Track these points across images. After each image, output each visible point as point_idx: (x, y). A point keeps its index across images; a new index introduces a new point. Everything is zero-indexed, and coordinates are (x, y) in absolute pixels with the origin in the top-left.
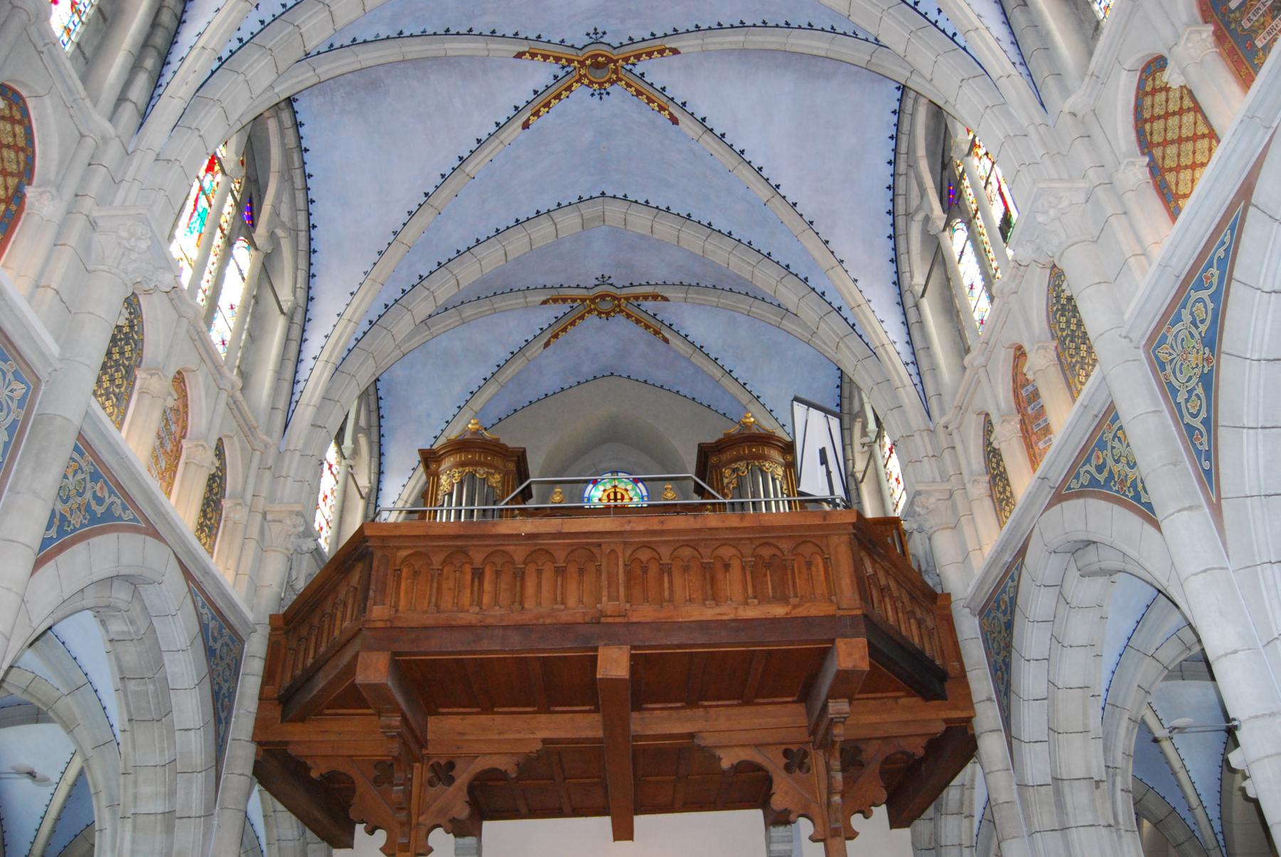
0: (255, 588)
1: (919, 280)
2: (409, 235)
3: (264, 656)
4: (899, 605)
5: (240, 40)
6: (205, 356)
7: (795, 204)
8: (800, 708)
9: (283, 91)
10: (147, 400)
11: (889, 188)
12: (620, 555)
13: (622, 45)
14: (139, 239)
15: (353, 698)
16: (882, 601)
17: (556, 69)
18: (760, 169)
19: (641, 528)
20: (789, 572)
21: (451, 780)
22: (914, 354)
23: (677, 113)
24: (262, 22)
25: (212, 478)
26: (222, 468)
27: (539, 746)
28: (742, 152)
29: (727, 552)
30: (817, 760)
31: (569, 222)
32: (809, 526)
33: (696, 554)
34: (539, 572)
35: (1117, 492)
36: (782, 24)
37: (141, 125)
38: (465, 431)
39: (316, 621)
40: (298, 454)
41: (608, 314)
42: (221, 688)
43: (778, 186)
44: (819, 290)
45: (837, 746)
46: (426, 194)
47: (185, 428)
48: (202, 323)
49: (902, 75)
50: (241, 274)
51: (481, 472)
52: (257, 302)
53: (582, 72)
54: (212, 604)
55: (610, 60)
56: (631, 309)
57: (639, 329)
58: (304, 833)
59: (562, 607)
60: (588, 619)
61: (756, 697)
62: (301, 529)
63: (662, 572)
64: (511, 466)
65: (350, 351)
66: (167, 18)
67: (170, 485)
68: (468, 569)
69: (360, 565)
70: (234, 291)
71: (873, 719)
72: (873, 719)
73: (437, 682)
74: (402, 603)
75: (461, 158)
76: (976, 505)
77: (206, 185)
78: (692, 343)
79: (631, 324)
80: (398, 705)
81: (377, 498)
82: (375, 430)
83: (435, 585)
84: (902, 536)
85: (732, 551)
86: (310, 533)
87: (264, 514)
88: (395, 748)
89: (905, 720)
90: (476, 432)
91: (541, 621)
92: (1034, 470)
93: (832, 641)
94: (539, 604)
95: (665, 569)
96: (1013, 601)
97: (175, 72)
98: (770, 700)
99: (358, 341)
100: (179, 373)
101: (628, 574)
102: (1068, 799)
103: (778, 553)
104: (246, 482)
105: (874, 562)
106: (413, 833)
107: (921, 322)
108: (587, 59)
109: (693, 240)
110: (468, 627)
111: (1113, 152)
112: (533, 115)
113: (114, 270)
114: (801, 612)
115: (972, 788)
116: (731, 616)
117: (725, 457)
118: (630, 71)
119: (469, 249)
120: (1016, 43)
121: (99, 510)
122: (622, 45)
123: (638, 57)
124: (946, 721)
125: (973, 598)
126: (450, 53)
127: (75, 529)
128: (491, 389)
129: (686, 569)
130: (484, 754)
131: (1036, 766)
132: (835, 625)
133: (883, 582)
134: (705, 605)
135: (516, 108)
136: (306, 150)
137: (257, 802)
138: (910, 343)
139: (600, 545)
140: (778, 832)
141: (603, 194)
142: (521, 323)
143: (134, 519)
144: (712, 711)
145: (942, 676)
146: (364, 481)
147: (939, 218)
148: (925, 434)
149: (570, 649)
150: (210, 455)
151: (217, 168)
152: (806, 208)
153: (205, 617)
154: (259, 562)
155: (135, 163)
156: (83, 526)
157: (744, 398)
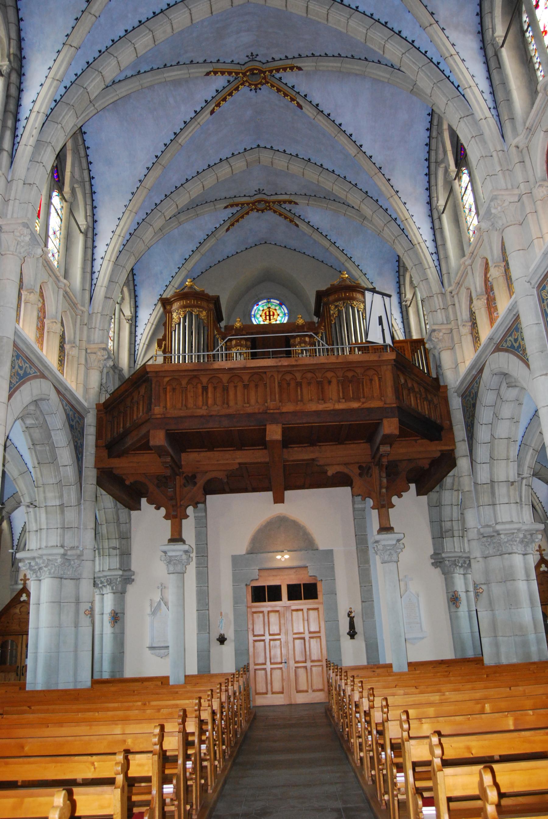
0: (86, 390)
1: (442, 202)
3: (95, 425)
7: (371, 157)
8: (366, 446)
10: (29, 305)
11: (426, 145)
12: (276, 378)
13: (268, 62)
14: (25, 236)
15: (145, 446)
16: (409, 395)
18: (351, 135)
19: (286, 364)
21: (195, 484)
22: (436, 247)
26: (64, 332)
27: (238, 466)
28: (340, 125)
29: (329, 375)
31: (239, 164)
34: (236, 387)
35: (522, 354)
36: (363, 58)
37: (12, 163)
40: (99, 315)
42: (77, 443)
43: (361, 146)
46: (156, 157)
47: (45, 312)
51: (195, 311)
53: (245, 79)
54: (72, 406)
55: (261, 72)
56: (276, 207)
57: (281, 219)
58: (116, 504)
59: (248, 405)
60: (261, 411)
62: (106, 357)
64: (212, 306)
65: (120, 252)
66: (13, 91)
67: (42, 344)
68: (200, 386)
76: (463, 338)
78: (312, 227)
81: (136, 322)
83: (184, 395)
85: (332, 374)
87: (86, 349)
90: (191, 287)
91: (238, 412)
92: (492, 327)
93: (382, 420)
96: (476, 394)
97: (24, 127)
99: (124, 245)
101: (280, 386)
102: (497, 491)
103: (355, 374)
104: (75, 334)
106: (179, 510)
107: (441, 229)
108: (247, 71)
109: (312, 175)
110: (202, 416)
111: (534, 175)
112: (216, 106)
113: (15, 253)
114: (366, 405)
116: (332, 408)
117: (331, 298)
119: (182, 185)
120: (493, 93)
121: (21, 372)
124: (441, 451)
125: (458, 389)
127: (15, 385)
128: (197, 257)
129: (309, 384)
130: (211, 471)
131: (483, 475)
132: (384, 412)
134: (318, 403)
135: (206, 101)
136: (85, 133)
138: (435, 240)
139: (265, 373)
142: (213, 218)
143: (35, 372)
147: (453, 171)
148: (439, 295)
150: (59, 325)
152: (378, 159)
154: (87, 375)
155: (14, 188)
156: (17, 382)
157: (343, 259)
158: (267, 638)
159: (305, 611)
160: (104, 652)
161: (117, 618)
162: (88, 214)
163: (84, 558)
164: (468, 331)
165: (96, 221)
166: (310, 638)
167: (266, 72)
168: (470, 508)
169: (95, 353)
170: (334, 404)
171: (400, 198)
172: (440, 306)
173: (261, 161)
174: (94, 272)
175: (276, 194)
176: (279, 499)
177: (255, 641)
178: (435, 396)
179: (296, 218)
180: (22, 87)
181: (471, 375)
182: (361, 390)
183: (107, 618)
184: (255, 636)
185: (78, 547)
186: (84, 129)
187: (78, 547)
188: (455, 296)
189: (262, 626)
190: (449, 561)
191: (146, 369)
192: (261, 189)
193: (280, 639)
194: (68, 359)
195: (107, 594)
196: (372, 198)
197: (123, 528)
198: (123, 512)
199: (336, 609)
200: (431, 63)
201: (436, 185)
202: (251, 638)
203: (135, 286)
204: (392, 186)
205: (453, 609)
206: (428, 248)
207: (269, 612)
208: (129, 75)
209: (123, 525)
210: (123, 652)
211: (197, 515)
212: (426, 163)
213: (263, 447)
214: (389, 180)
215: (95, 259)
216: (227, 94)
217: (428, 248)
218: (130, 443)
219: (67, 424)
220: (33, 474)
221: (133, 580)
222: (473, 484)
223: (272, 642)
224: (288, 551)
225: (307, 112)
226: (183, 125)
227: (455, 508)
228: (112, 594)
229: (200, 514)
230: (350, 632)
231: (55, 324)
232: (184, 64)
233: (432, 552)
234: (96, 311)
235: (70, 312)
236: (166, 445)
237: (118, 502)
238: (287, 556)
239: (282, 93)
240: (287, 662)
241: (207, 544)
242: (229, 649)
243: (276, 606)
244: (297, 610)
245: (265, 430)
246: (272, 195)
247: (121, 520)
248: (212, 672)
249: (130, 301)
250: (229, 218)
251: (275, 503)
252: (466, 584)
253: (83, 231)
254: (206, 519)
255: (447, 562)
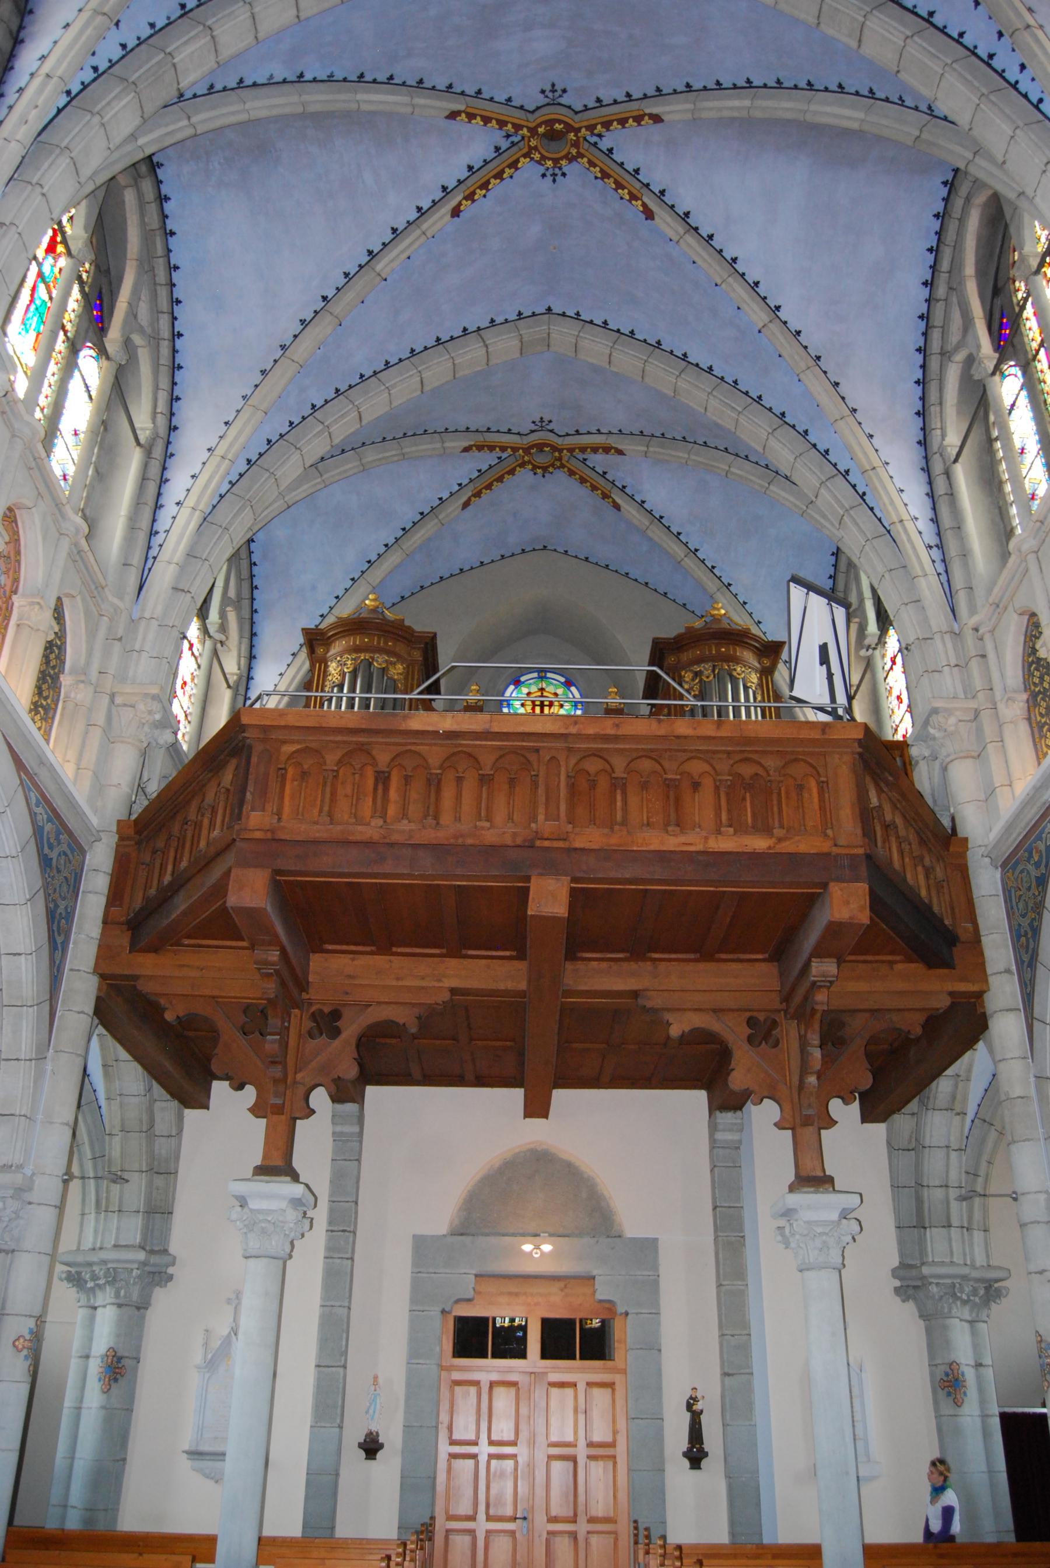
0: (99, 787)
1: (953, 439)
2: (301, 350)
4: (905, 847)
5: (95, 69)
6: (43, 489)
7: (798, 333)
9: (148, 143)
11: (921, 317)
13: (586, 108)
15: (222, 925)
16: (886, 840)
17: (495, 136)
18: (757, 284)
19: (591, 731)
20: (775, 797)
22: (939, 534)
23: (652, 205)
24: (124, 46)
25: (49, 646)
26: (61, 635)
27: (446, 996)
28: (734, 260)
29: (697, 767)
30: (789, 1032)
31: (504, 345)
32: (802, 740)
33: (658, 767)
34: (459, 780)
36: (803, 84)
38: (361, 606)
39: (176, 830)
40: (154, 623)
41: (545, 469)
42: (57, 906)
43: (778, 308)
44: (822, 447)
45: (818, 1016)
46: (324, 298)
47: (16, 580)
48: (40, 447)
49: (958, 155)
50: (89, 391)
51: (379, 661)
52: (106, 429)
53: (533, 143)
55: (569, 128)
56: (574, 464)
57: (584, 491)
59: (488, 824)
60: (519, 841)
61: (720, 951)
62: (158, 717)
63: (614, 787)
64: (417, 655)
65: (222, 497)
69: (234, 762)
70: (78, 414)
71: (862, 986)
72: (862, 986)
73: (324, 912)
74: (287, 810)
75: (370, 252)
76: (1008, 731)
77: (46, 269)
79: (573, 483)
80: (276, 936)
82: (246, 603)
83: (328, 789)
84: (907, 766)
86: (169, 723)
87: (112, 696)
88: (271, 988)
89: (904, 990)
90: (374, 610)
91: (460, 841)
93: (825, 886)
94: (458, 819)
95: (617, 785)
97: (11, 107)
98: (736, 956)
99: (232, 484)
100: (10, 509)
101: (572, 788)
103: (761, 772)
105: (880, 791)
107: (952, 495)
108: (539, 125)
109: (662, 375)
110: (369, 844)
114: (787, 847)
115: (968, 1080)
116: (700, 847)
117: (685, 657)
118: (595, 144)
119: (375, 373)
122: (586, 108)
123: (607, 125)
124: (951, 994)
125: (994, 847)
126: (365, 107)
128: (394, 558)
129: (644, 786)
132: (827, 868)
133: (888, 817)
135: (444, 188)
136: (172, 233)
137: (102, 1047)
138: (935, 520)
139: (537, 750)
140: (726, 1118)
141: (549, 309)
142: (433, 476)
144: (662, 966)
145: (952, 939)
146: (232, 665)
147: (989, 358)
148: (947, 637)
149: (495, 878)
150: (48, 614)
151: (60, 248)
152: (814, 338)
153: (39, 817)
154: (105, 756)
158: (484, 1450)
159: (581, 1387)
160: (77, 1455)
161: (118, 1369)
162: (159, 410)
163: (34, 1196)
164: (1019, 712)
165: (176, 428)
166: (589, 1457)
167: (579, 130)
168: (1028, 1140)
169: (133, 707)
170: (706, 838)
171: (860, 423)
172: (948, 660)
173: (552, 342)
174: (157, 533)
175: (577, 432)
176: (537, 1107)
177: (453, 1456)
178: (938, 860)
179: (615, 489)
180: (22, 35)
181: (1039, 804)
182: (776, 809)
183: (95, 1367)
184: (453, 1443)
185: (20, 1167)
186: (155, 159)
187: (20, 1167)
188: (987, 638)
189: (472, 1419)
190: (937, 1284)
191: (239, 718)
192: (546, 419)
193: (513, 1457)
194: (64, 708)
195: (104, 1306)
196: (793, 427)
197: (162, 1147)
198: (166, 1107)
199: (659, 1388)
200: (973, 58)
201: (941, 404)
202: (444, 1449)
203: (254, 611)
204: (843, 398)
205: (947, 1408)
206: (920, 533)
207: (492, 1385)
208: (278, 78)
209: (163, 1140)
210: (124, 1460)
211: (339, 1129)
212: (919, 358)
213: (514, 953)
214: (837, 384)
215: (162, 506)
216: (492, 174)
217: (920, 533)
218: (183, 907)
219: (32, 848)
220: (104, 1110)
221: (170, 1278)
222: (1032, 1079)
223: (493, 1462)
224: (551, 1235)
225: (663, 227)
226: (388, 236)
227: (954, 1155)
228: (114, 1308)
229: (347, 1129)
230: (690, 1450)
231: (37, 607)
232: (404, 84)
233: (895, 1262)
234: (147, 615)
235: (83, 600)
236: (269, 908)
237: (154, 1083)
238: (547, 1248)
239: (612, 180)
240: (530, 1517)
241: (356, 1203)
242: (387, 1469)
243: (510, 1371)
244: (562, 1385)
245: (526, 891)
246: (568, 435)
247: (160, 1128)
248: (341, 1532)
249: (240, 643)
250: (471, 481)
251: (525, 1117)
252: (976, 1346)
253: (142, 441)
254: (361, 1142)
255: (934, 1289)
